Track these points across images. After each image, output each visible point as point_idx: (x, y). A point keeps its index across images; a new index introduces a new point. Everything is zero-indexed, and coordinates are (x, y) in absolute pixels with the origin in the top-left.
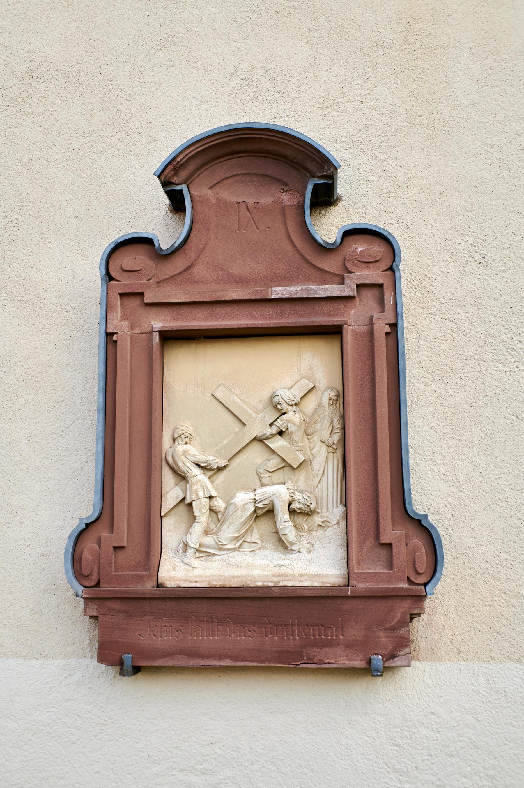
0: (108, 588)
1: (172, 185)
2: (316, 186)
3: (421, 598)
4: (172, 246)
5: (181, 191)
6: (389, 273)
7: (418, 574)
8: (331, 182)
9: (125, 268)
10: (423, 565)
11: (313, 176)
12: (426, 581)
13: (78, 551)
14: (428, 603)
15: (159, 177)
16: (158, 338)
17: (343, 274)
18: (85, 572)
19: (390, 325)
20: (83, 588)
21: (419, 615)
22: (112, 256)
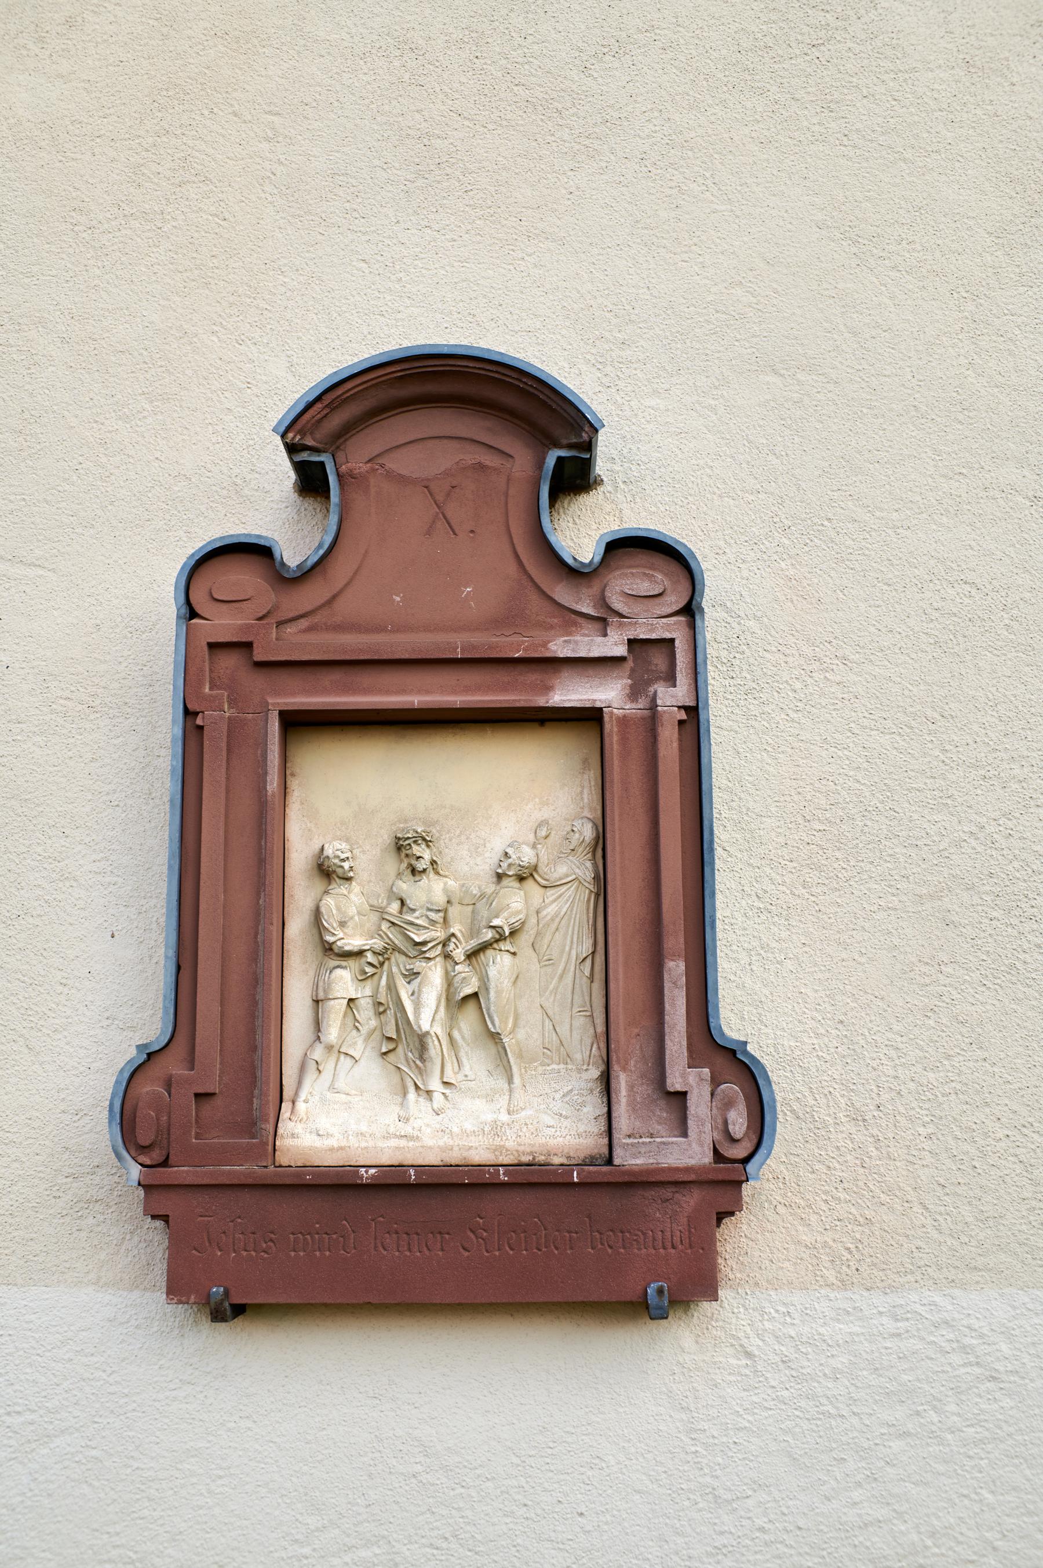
0: (182, 1172)
2: (560, 460)
3: (737, 1184)
5: (322, 464)
7: (734, 1141)
8: (588, 456)
9: (216, 596)
10: (739, 1122)
11: (557, 445)
14: (747, 1189)
15: (283, 436)
16: (277, 724)
17: (605, 616)
20: (140, 1167)
21: (732, 1214)
22: (196, 574)
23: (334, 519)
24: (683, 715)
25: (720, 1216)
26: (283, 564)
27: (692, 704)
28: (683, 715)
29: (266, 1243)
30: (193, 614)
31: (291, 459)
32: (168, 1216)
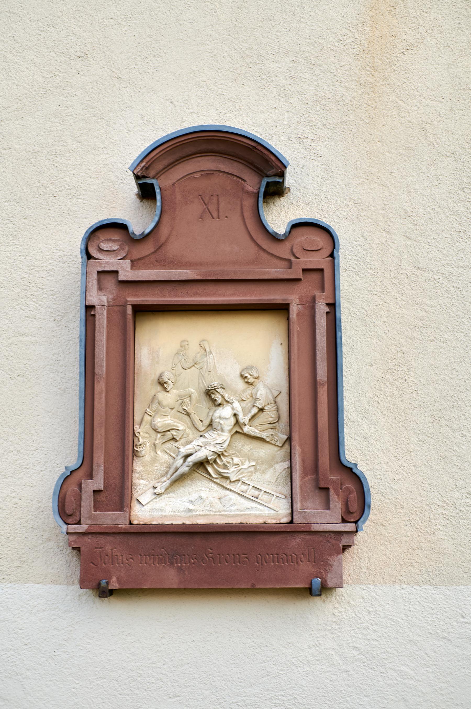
1: (147, 179)
4: (143, 233)
6: (330, 259)
12: (357, 519)
13: (63, 491)
18: (69, 511)
19: (328, 304)
21: (349, 546)
23: (158, 212)
24: (328, 310)
25: (345, 547)
26: (133, 233)
27: (331, 301)
28: (328, 310)
29: (193, 560)
30: (89, 257)
31: (136, 182)
32: (79, 548)
